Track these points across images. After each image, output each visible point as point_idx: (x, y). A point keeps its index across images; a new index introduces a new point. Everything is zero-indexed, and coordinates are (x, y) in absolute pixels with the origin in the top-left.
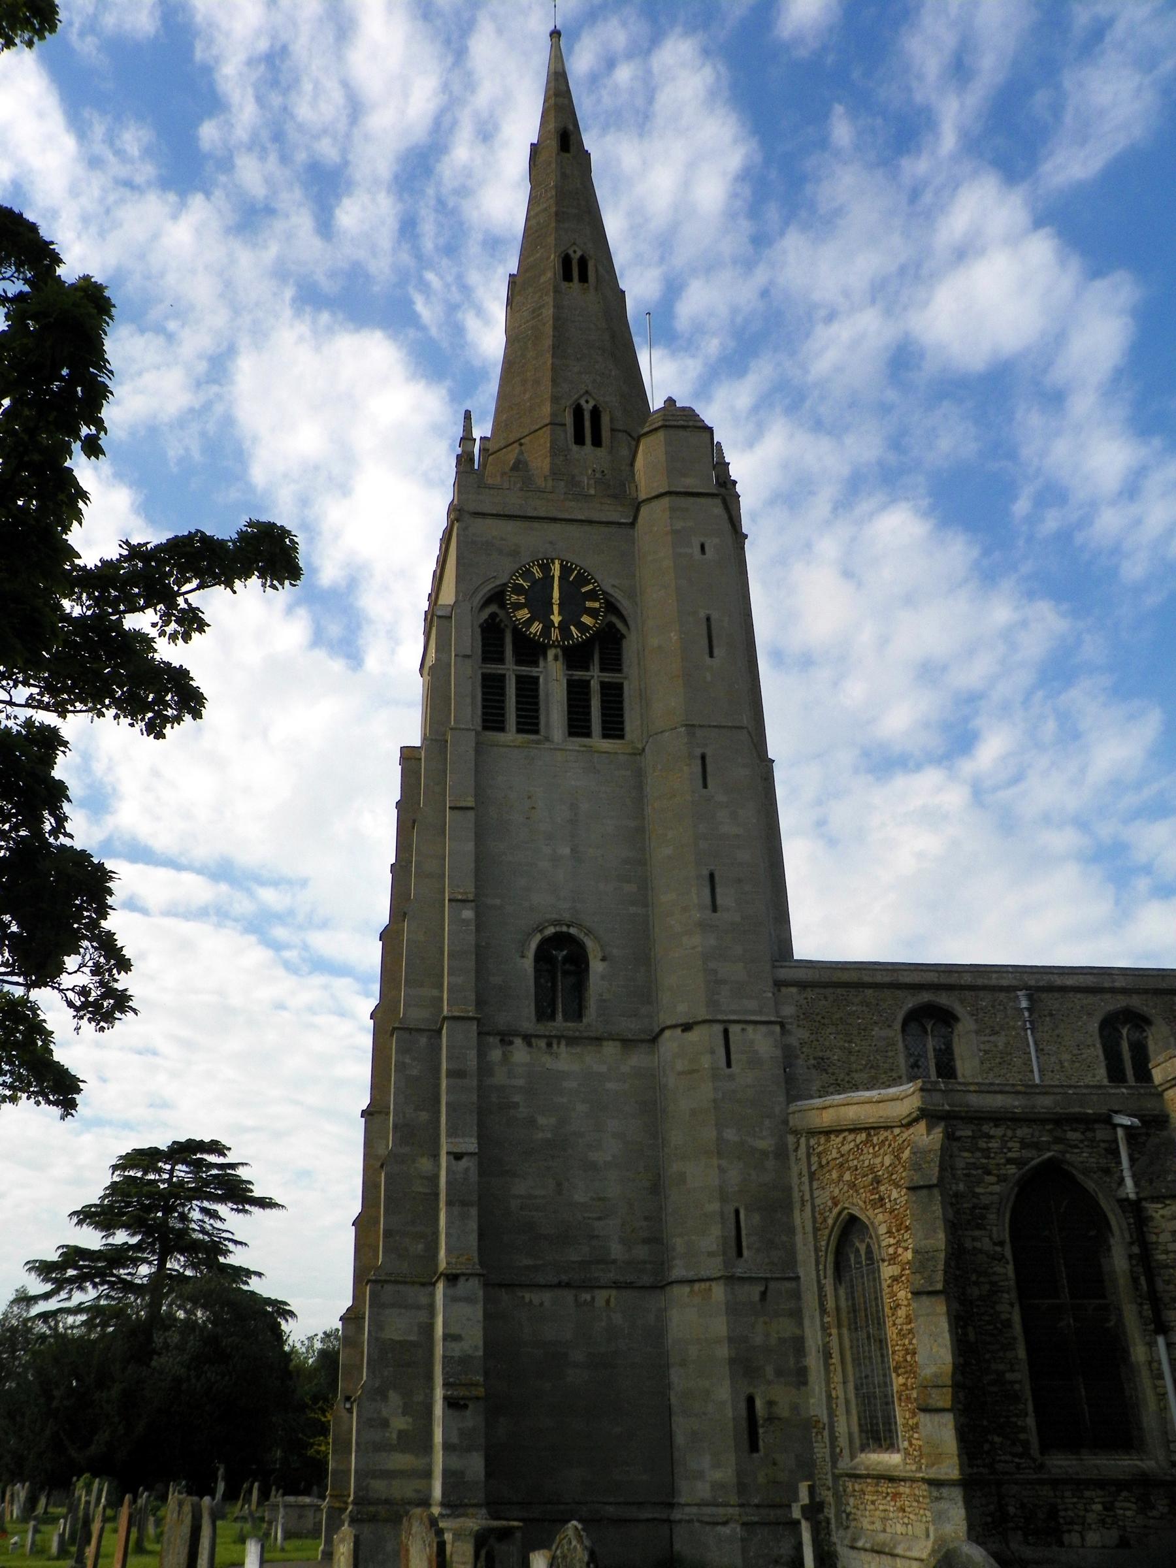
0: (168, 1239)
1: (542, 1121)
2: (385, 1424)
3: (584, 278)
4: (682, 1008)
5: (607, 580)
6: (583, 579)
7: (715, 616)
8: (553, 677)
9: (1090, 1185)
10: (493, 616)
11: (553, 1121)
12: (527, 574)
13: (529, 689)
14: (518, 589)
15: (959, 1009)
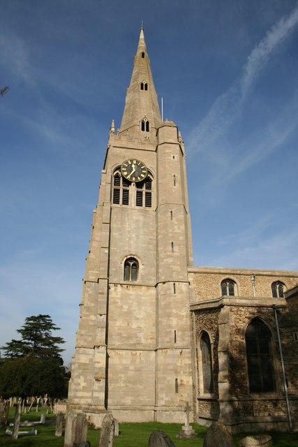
0: (37, 338)
1: (124, 307)
2: (79, 384)
3: (146, 89)
4: (163, 278)
5: (148, 166)
6: (142, 165)
7: (176, 175)
8: (133, 190)
9: (266, 323)
10: (117, 173)
11: (127, 307)
12: (127, 163)
13: (126, 192)
14: (124, 167)
15: (235, 280)
